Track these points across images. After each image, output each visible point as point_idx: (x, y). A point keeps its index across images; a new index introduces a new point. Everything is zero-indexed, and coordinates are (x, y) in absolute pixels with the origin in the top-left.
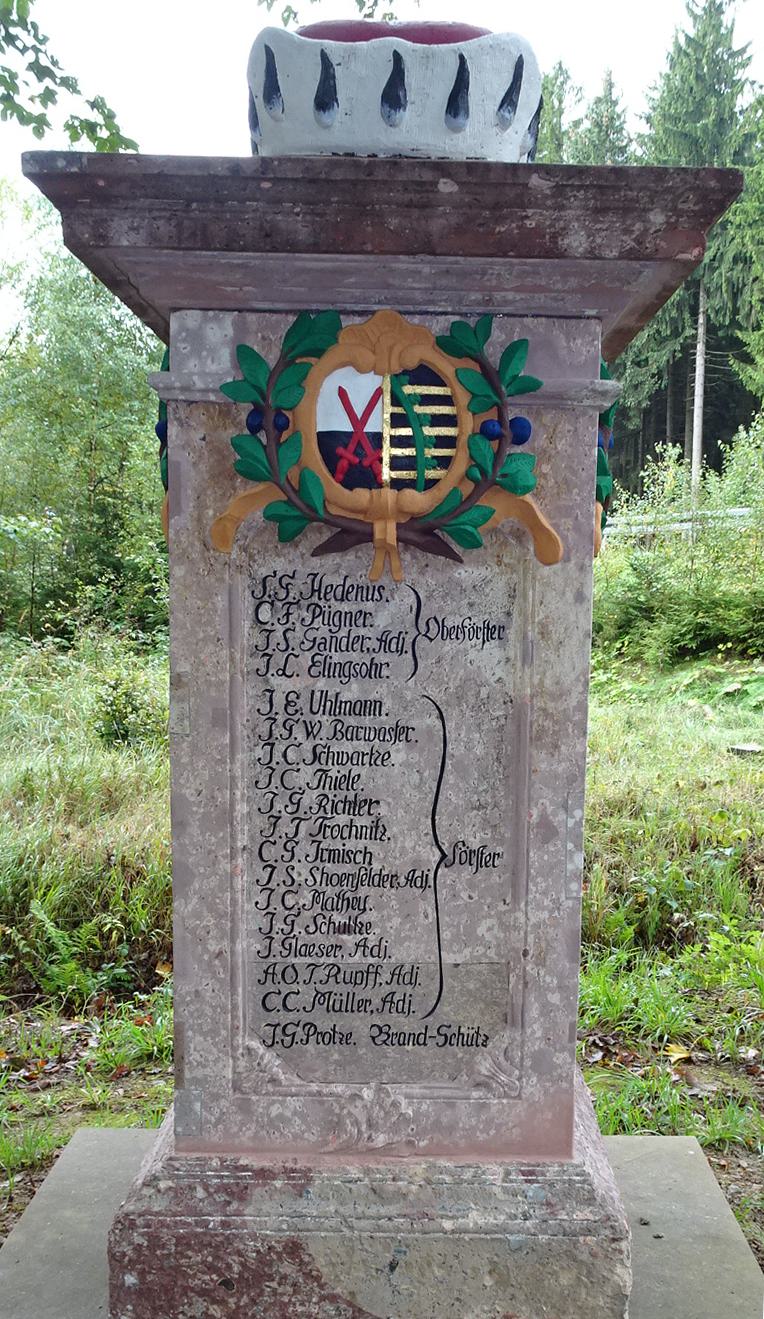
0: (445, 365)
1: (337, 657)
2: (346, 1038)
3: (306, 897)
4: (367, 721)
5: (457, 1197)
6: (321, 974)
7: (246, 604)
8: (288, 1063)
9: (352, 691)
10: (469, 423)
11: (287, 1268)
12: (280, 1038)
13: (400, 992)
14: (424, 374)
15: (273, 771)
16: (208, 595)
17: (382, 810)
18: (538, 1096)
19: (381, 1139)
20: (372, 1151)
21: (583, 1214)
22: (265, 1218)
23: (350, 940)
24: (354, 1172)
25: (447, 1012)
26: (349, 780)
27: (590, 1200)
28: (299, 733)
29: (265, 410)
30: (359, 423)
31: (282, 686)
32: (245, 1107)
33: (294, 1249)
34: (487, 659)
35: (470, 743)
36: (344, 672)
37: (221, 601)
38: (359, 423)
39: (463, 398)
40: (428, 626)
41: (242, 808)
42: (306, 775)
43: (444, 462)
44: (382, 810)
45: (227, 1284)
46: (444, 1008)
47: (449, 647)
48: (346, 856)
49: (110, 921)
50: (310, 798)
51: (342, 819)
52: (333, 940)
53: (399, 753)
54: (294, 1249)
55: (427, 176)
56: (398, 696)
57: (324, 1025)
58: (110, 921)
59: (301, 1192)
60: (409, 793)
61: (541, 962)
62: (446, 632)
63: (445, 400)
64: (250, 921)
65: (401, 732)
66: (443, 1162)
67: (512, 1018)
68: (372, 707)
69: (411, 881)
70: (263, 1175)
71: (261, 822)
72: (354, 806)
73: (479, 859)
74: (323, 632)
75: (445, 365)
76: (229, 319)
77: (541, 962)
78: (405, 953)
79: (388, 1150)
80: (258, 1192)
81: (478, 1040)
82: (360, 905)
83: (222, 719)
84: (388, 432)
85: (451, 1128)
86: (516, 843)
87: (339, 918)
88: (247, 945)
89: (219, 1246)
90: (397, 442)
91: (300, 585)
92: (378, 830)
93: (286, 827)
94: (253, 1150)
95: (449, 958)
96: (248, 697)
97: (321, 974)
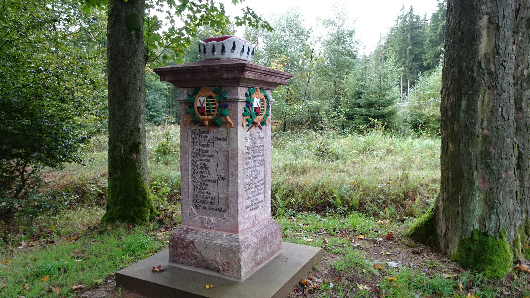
0: (214, 95)
1: (203, 143)
2: (205, 208)
3: (199, 184)
4: (207, 154)
5: (218, 238)
6: (202, 197)
7: (190, 134)
8: (197, 211)
9: (205, 149)
10: (217, 104)
11: (192, 246)
12: (196, 207)
13: (213, 201)
14: (211, 97)
15: (194, 162)
16: (185, 133)
17: (209, 169)
18: (233, 222)
19: (209, 227)
20: (208, 228)
21: (236, 244)
22: (190, 237)
23: (205, 191)
24: (204, 232)
25: (220, 205)
26: (204, 164)
27: (237, 242)
28: (198, 156)
29: (191, 104)
30: (202, 105)
31: (195, 148)
32: (191, 218)
33: (192, 242)
34: (224, 144)
35: (222, 159)
36: (204, 146)
37: (186, 134)
38: (202, 105)
39: (216, 101)
40: (216, 139)
41: (190, 168)
42: (198, 163)
43: (214, 111)
44: (209, 169)
45: (184, 247)
46: (219, 205)
47: (218, 142)
48: (204, 177)
49: (293, 200)
50: (199, 167)
51: (204, 170)
52: (203, 191)
53: (212, 160)
54: (192, 242)
55: (202, 68)
56: (211, 150)
57: (202, 206)
58: (293, 200)
59: (196, 233)
60: (213, 167)
61: (232, 198)
62: (219, 139)
63: (214, 101)
64: (191, 187)
65: (212, 156)
66: (218, 232)
67: (229, 208)
68: (207, 152)
69: (214, 182)
70: (192, 230)
71: (193, 170)
72: (205, 168)
73: (223, 179)
74: (201, 139)
75: (214, 95)
76: (187, 89)
77: (232, 198)
78: (214, 194)
79: (210, 228)
80: (190, 232)
81: (224, 211)
82: (206, 185)
83: (187, 153)
84: (206, 106)
85: (220, 226)
86: (228, 176)
87: (204, 187)
88: (191, 191)
89: (183, 240)
90: (207, 108)
91: (198, 131)
92: (209, 172)
93: (196, 172)
94: (192, 226)
95: (220, 196)
96: (190, 149)
97: (202, 197)
